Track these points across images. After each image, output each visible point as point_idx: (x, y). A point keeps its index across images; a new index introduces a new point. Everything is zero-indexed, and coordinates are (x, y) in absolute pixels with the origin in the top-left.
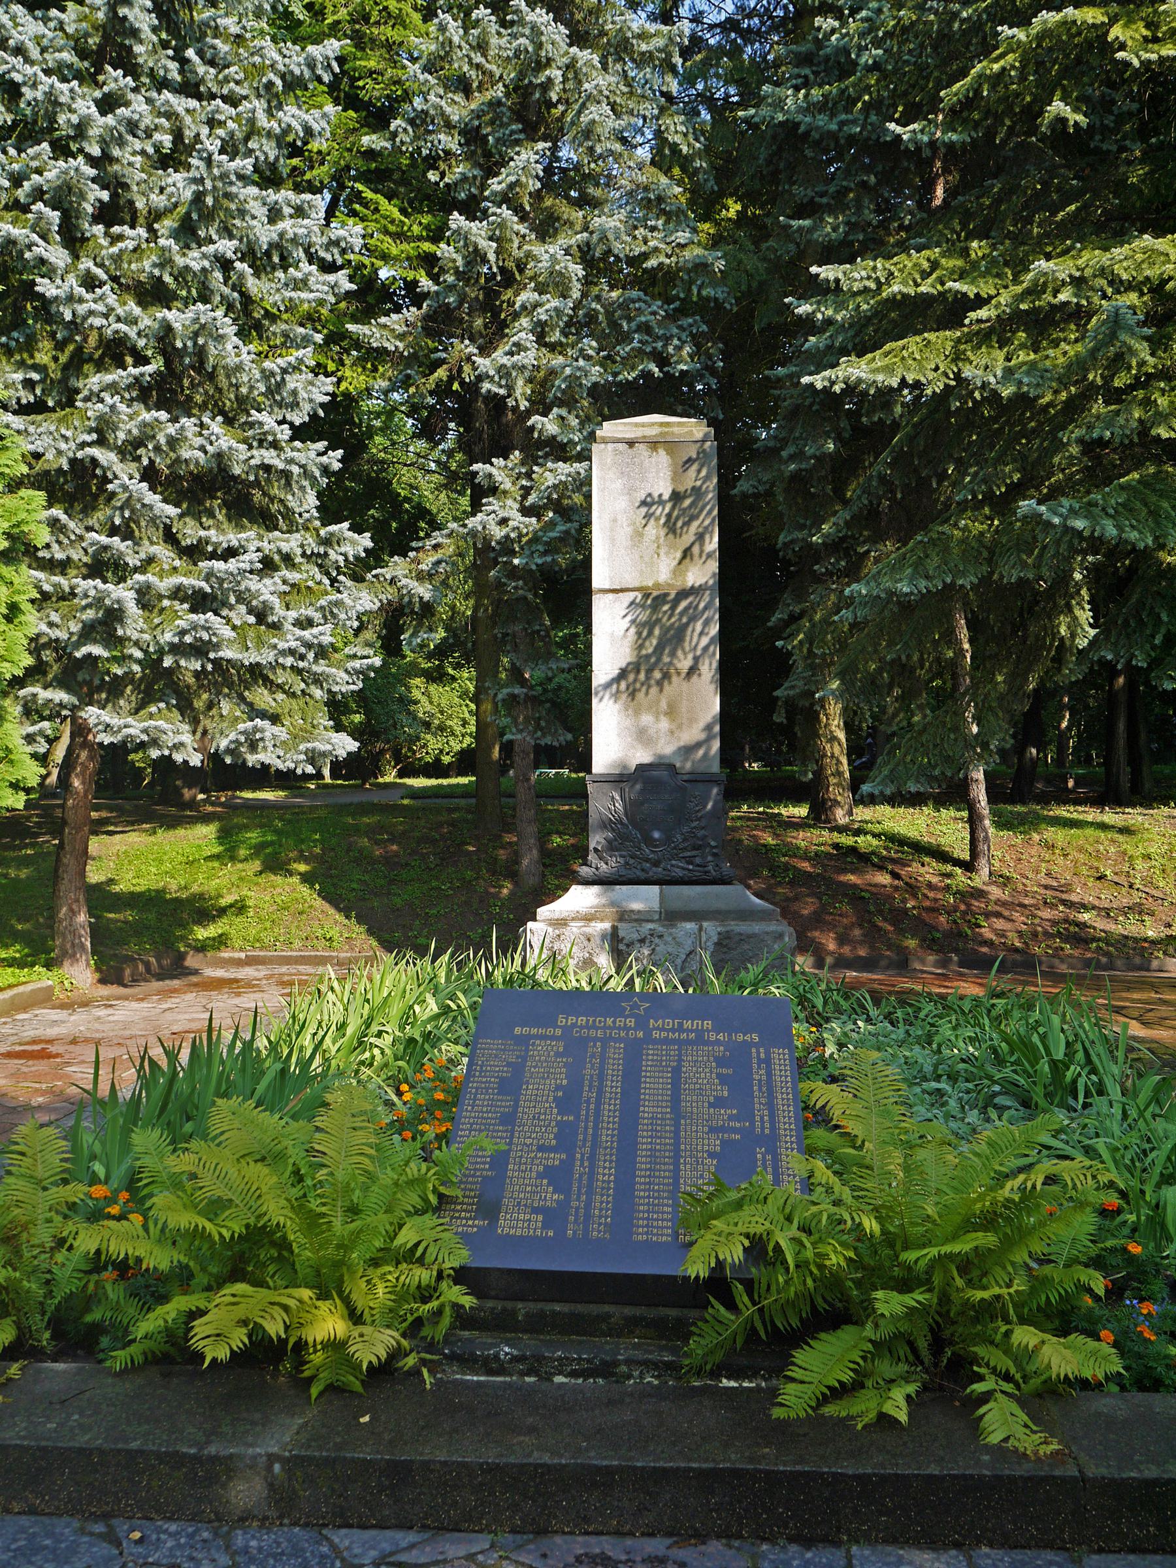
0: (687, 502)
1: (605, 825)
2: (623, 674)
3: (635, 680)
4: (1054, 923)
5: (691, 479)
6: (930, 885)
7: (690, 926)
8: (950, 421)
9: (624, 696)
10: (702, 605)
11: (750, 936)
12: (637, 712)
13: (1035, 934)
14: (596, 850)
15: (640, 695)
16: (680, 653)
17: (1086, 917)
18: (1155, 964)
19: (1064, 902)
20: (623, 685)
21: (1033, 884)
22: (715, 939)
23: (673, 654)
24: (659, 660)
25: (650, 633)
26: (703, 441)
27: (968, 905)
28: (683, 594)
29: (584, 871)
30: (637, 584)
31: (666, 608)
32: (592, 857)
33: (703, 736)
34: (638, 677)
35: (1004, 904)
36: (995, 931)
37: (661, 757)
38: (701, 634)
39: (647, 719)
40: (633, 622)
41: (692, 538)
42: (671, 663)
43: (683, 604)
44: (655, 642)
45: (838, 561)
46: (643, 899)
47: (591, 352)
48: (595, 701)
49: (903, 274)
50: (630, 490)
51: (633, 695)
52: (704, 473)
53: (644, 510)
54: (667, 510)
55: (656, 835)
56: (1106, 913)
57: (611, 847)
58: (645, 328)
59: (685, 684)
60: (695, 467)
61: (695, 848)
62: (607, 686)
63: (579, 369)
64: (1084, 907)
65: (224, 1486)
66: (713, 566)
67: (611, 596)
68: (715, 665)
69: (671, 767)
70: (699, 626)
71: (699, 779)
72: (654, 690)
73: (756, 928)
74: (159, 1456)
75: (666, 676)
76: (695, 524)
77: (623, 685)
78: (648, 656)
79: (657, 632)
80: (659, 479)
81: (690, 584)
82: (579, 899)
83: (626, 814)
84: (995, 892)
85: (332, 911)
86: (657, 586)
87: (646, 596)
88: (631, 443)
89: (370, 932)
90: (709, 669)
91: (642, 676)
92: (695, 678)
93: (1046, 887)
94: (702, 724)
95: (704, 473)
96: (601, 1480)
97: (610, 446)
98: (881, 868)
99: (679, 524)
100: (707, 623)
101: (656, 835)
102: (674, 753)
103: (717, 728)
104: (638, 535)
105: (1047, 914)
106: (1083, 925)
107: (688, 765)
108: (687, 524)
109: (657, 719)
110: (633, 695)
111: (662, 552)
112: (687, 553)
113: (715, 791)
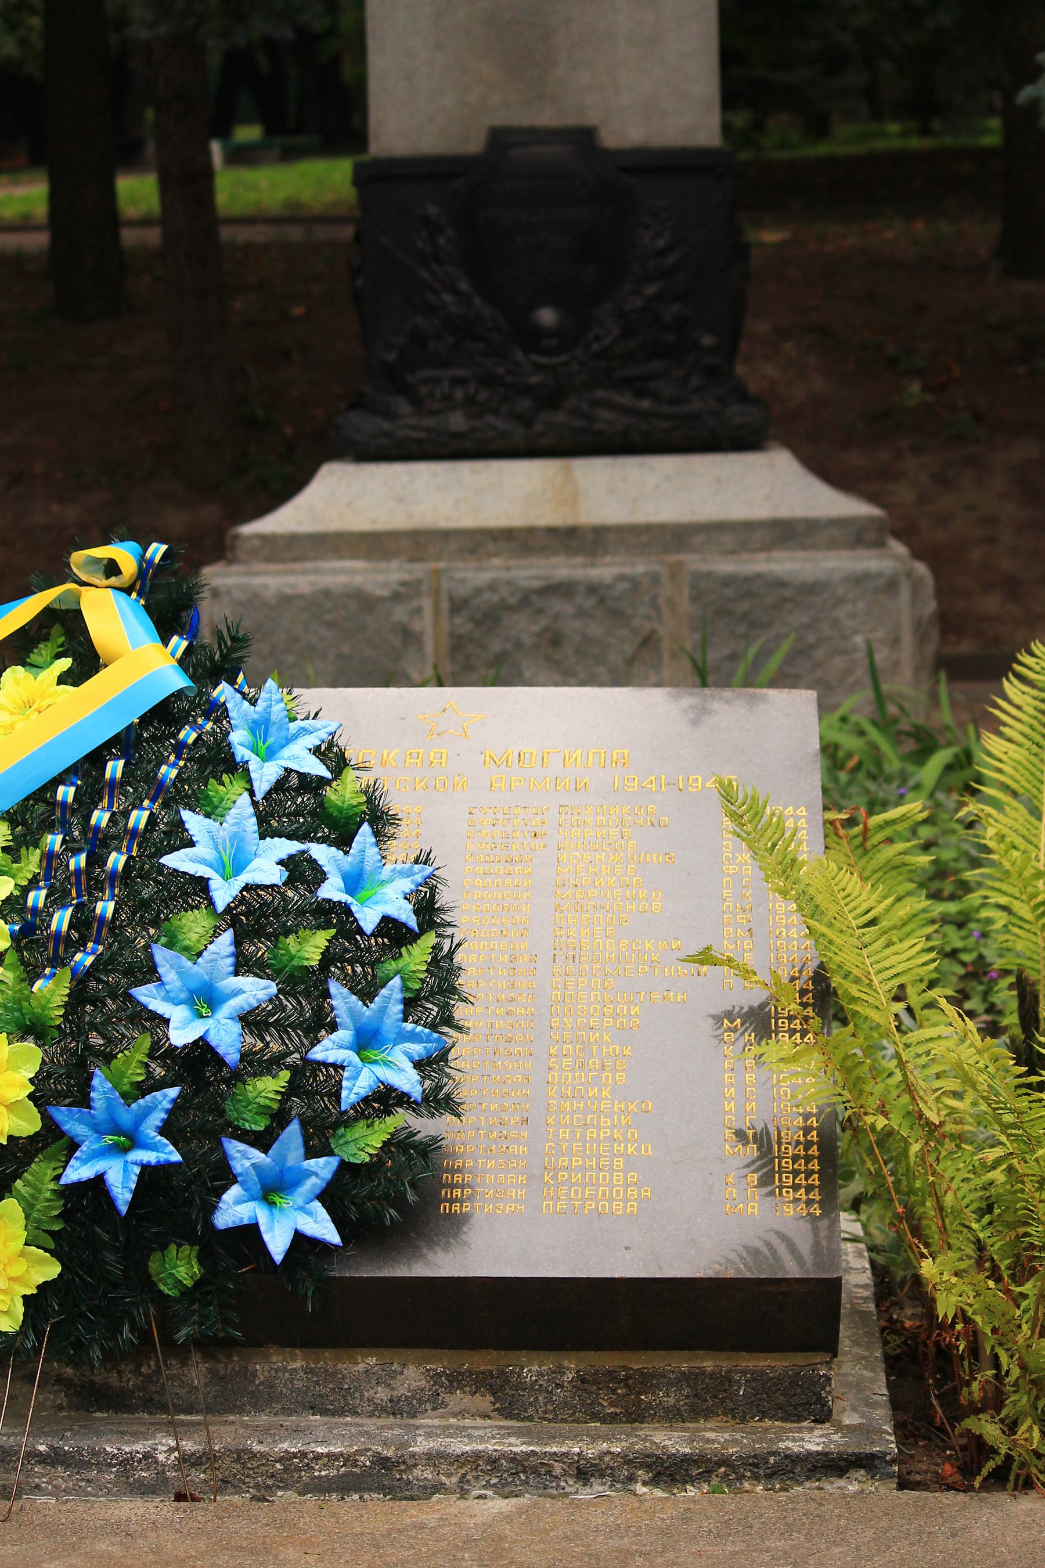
11: (812, 588)
55: (547, 316)
101: (547, 316)
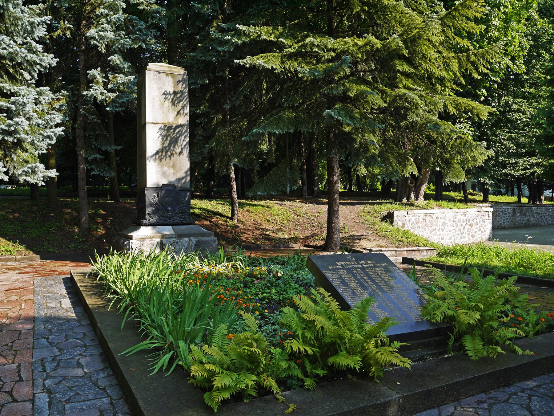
0: (179, 95)
1: (151, 205)
2: (157, 153)
3: (162, 155)
4: (261, 235)
5: (180, 87)
6: (221, 224)
7: (186, 239)
8: (285, 82)
9: (158, 161)
10: (184, 131)
12: (162, 166)
13: (257, 238)
14: (148, 214)
15: (163, 160)
16: (176, 146)
17: (268, 233)
18: (290, 245)
19: (261, 228)
20: (157, 156)
21: (250, 222)
22: (195, 243)
23: (174, 147)
24: (170, 148)
25: (167, 139)
26: (184, 75)
27: (235, 230)
28: (177, 127)
29: (145, 221)
30: (162, 122)
31: (172, 131)
32: (147, 216)
33: (184, 175)
34: (164, 153)
35: (245, 230)
36: (245, 238)
37: (170, 182)
38: (184, 140)
39: (165, 168)
40: (161, 135)
41: (180, 108)
42: (173, 150)
43: (178, 130)
44: (168, 142)
45: (204, 119)
46: (168, 230)
47: (122, 36)
48: (147, 162)
49: (265, 33)
50: (160, 89)
51: (161, 160)
52: (184, 86)
53: (164, 96)
54: (172, 97)
55: (169, 209)
56: (273, 231)
57: (154, 212)
58: (140, 30)
59: (178, 157)
60: (181, 83)
61: (182, 213)
62: (152, 156)
63: (126, 41)
64: (267, 230)
65: (388, 410)
66: (187, 118)
67: (153, 125)
68: (188, 151)
69: (174, 185)
70: (183, 138)
71: (183, 190)
72: (168, 159)
73: (208, 239)
74: (370, 406)
75: (172, 154)
76: (181, 103)
77: (157, 156)
78: (166, 147)
79: (169, 139)
80: (169, 86)
81: (179, 124)
82: (145, 232)
83: (159, 201)
84: (241, 226)
85: (4, 240)
86: (169, 123)
87: (165, 126)
88: (159, 73)
89: (26, 248)
90: (186, 152)
91: (164, 154)
92: (181, 155)
93: (254, 224)
94: (184, 171)
95: (184, 86)
96: (468, 382)
97: (152, 72)
98: (205, 219)
99: (176, 102)
100: (185, 137)
102: (175, 181)
103: (189, 173)
104: (162, 105)
105: (257, 232)
106: (268, 235)
107: (180, 185)
108: (179, 103)
109: (169, 169)
110: (161, 160)
111: (170, 111)
112: (179, 112)
113: (188, 194)
